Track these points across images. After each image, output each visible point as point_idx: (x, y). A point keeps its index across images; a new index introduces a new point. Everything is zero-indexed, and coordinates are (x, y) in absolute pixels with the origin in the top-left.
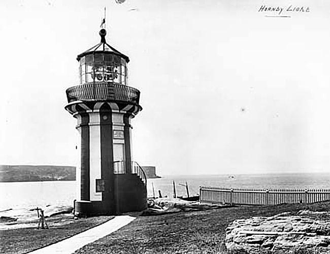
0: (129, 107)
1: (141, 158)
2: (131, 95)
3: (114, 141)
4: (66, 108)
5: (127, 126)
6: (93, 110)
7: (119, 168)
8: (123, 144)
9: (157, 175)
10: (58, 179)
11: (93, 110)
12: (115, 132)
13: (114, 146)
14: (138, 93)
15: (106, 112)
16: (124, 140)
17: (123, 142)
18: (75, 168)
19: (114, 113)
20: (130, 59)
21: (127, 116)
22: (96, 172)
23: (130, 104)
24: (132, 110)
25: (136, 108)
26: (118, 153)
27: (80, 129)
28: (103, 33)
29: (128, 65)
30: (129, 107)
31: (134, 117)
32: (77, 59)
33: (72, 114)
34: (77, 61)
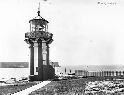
0: (49, 40)
1: (53, 59)
2: (49, 35)
5: (48, 47)
7: (45, 63)
13: (43, 55)
14: (52, 35)
15: (40, 42)
17: (46, 53)
21: (48, 43)
22: (36, 64)
23: (49, 39)
24: (50, 41)
25: (51, 40)
26: (44, 57)
27: (30, 48)
28: (39, 12)
30: (49, 40)
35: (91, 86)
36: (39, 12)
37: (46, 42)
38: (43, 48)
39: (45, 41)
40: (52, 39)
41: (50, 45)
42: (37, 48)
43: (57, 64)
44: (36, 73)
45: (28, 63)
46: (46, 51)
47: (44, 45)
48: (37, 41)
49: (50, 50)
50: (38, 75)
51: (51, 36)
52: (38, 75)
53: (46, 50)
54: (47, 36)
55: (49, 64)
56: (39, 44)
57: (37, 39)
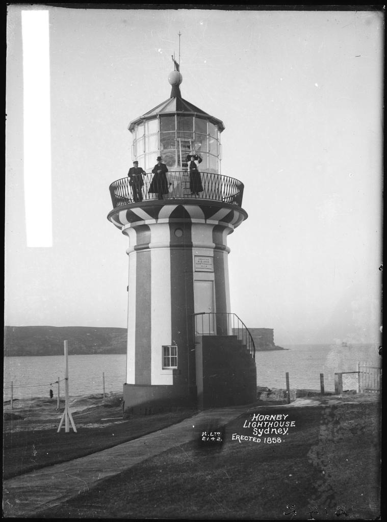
0: (224, 212)
1: (243, 313)
2: (227, 191)
3: (196, 276)
4: (108, 217)
5: (220, 248)
6: (157, 218)
7: (204, 326)
8: (213, 281)
9: (276, 345)
10: (99, 351)
11: (157, 218)
12: (197, 258)
13: (196, 285)
14: (241, 187)
15: (180, 224)
16: (213, 274)
17: (212, 276)
18: (126, 331)
19: (195, 224)
20: (225, 124)
21: (219, 229)
22: (162, 333)
23: (226, 211)
24: (229, 218)
25: (236, 214)
26: (203, 301)
27: (134, 254)
28: (176, 86)
29: (223, 136)
30: (224, 212)
31: (232, 231)
32: (323, 374)
33: (120, 228)
34: (322, 373)
35: (330, 378)
36: (176, 86)
37: (209, 221)
38: (195, 252)
39: (206, 218)
40: (243, 207)
41: (231, 240)
42: (196, 312)
43: (263, 339)
44: (162, 377)
45: (126, 331)
46: (211, 267)
47: (201, 237)
48: (167, 220)
49: (233, 264)
50: (171, 383)
51: (235, 191)
52: (171, 383)
53: (211, 260)
54: (218, 192)
55: (226, 330)
56: (179, 233)
57: (168, 209)
